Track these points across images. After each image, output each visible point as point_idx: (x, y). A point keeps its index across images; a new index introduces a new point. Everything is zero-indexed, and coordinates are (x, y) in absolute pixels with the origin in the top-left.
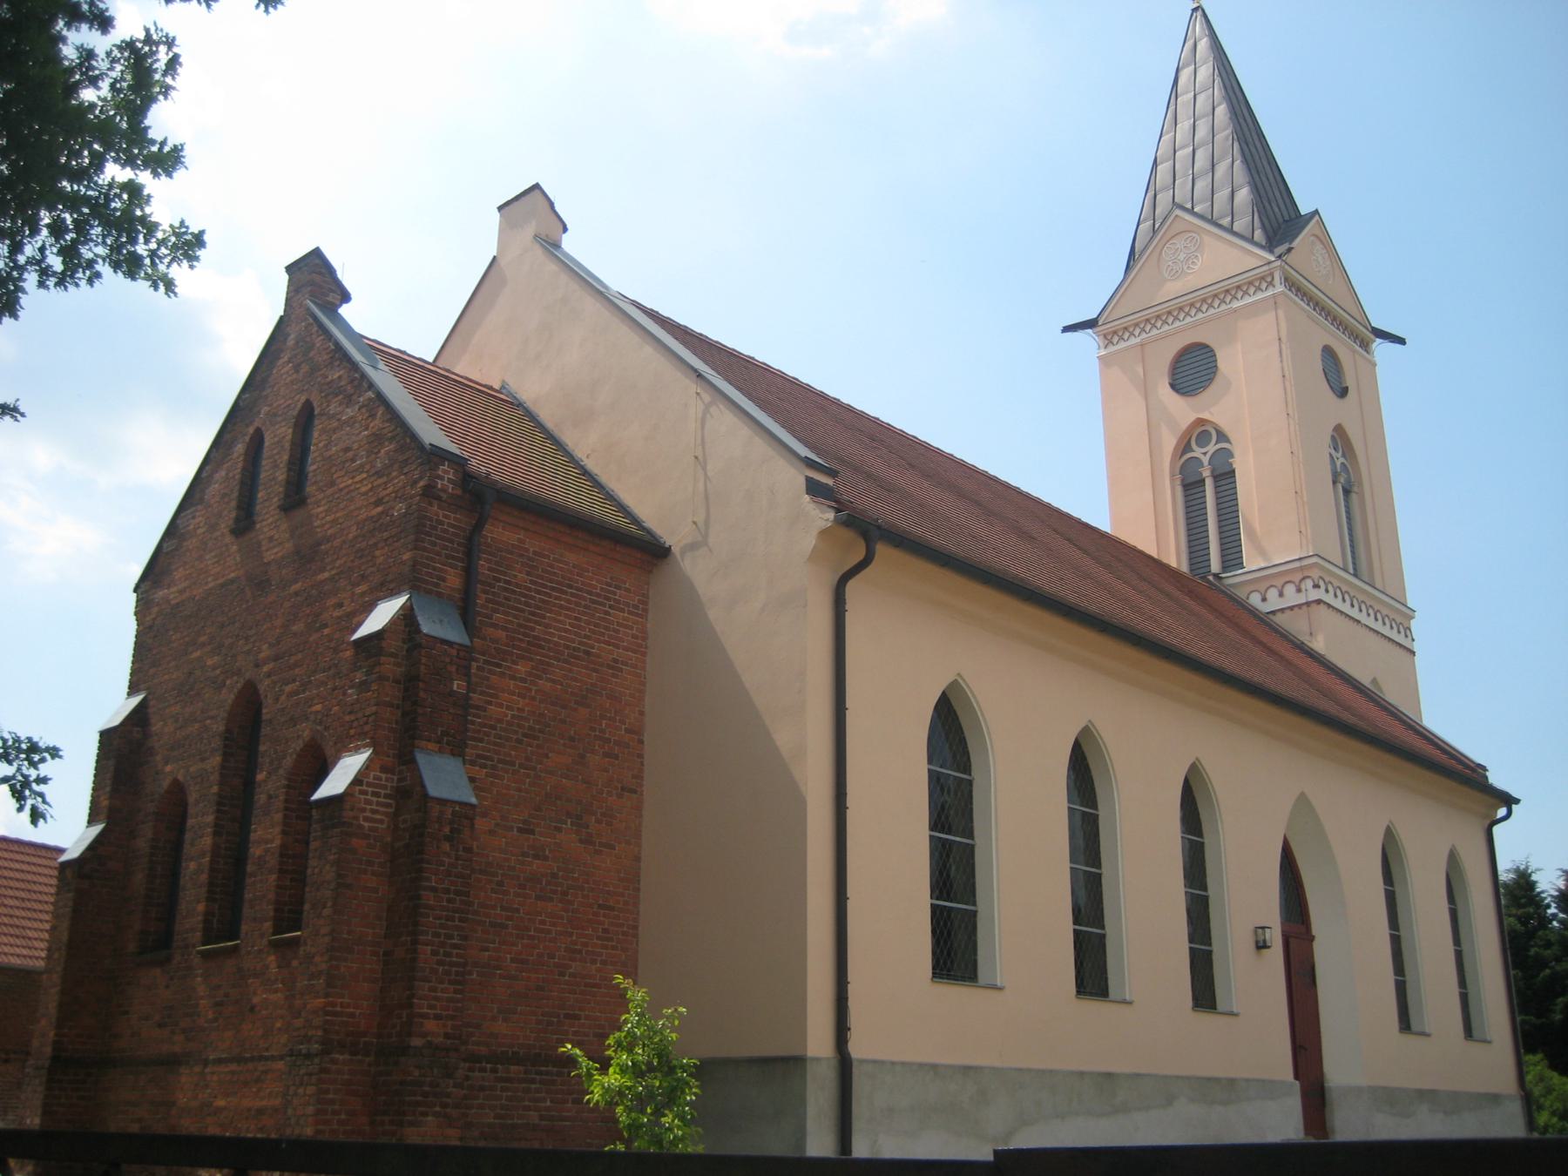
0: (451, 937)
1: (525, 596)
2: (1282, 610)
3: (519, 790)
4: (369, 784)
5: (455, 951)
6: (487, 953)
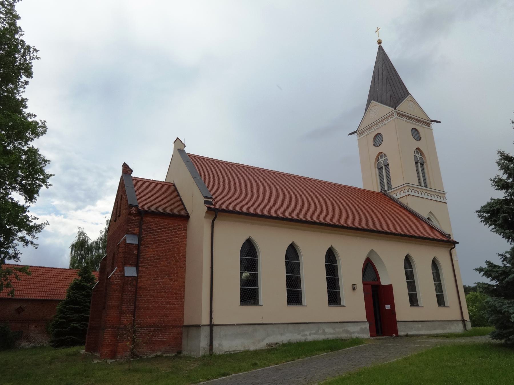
0: (131, 304)
1: (155, 231)
2: (401, 198)
3: (154, 271)
4: (116, 274)
5: (131, 307)
6: (145, 305)
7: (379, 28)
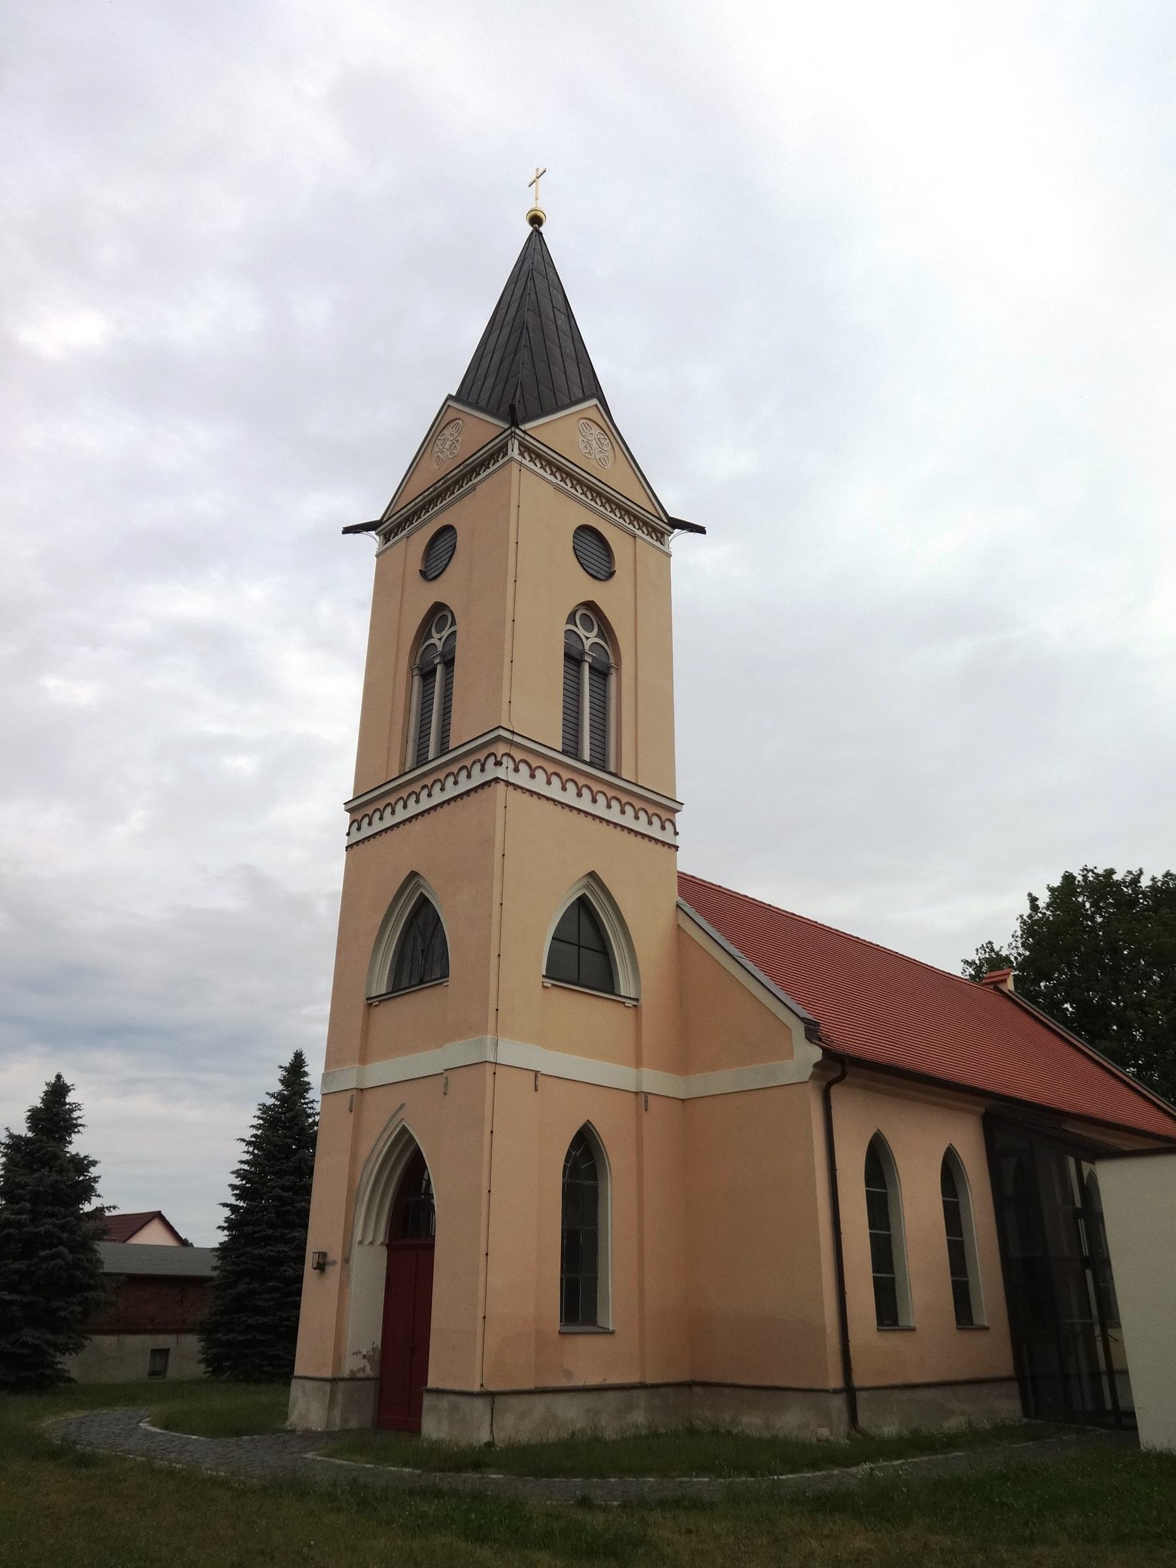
7: (540, 171)
